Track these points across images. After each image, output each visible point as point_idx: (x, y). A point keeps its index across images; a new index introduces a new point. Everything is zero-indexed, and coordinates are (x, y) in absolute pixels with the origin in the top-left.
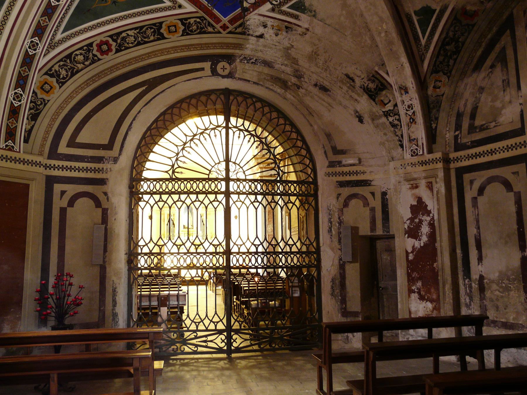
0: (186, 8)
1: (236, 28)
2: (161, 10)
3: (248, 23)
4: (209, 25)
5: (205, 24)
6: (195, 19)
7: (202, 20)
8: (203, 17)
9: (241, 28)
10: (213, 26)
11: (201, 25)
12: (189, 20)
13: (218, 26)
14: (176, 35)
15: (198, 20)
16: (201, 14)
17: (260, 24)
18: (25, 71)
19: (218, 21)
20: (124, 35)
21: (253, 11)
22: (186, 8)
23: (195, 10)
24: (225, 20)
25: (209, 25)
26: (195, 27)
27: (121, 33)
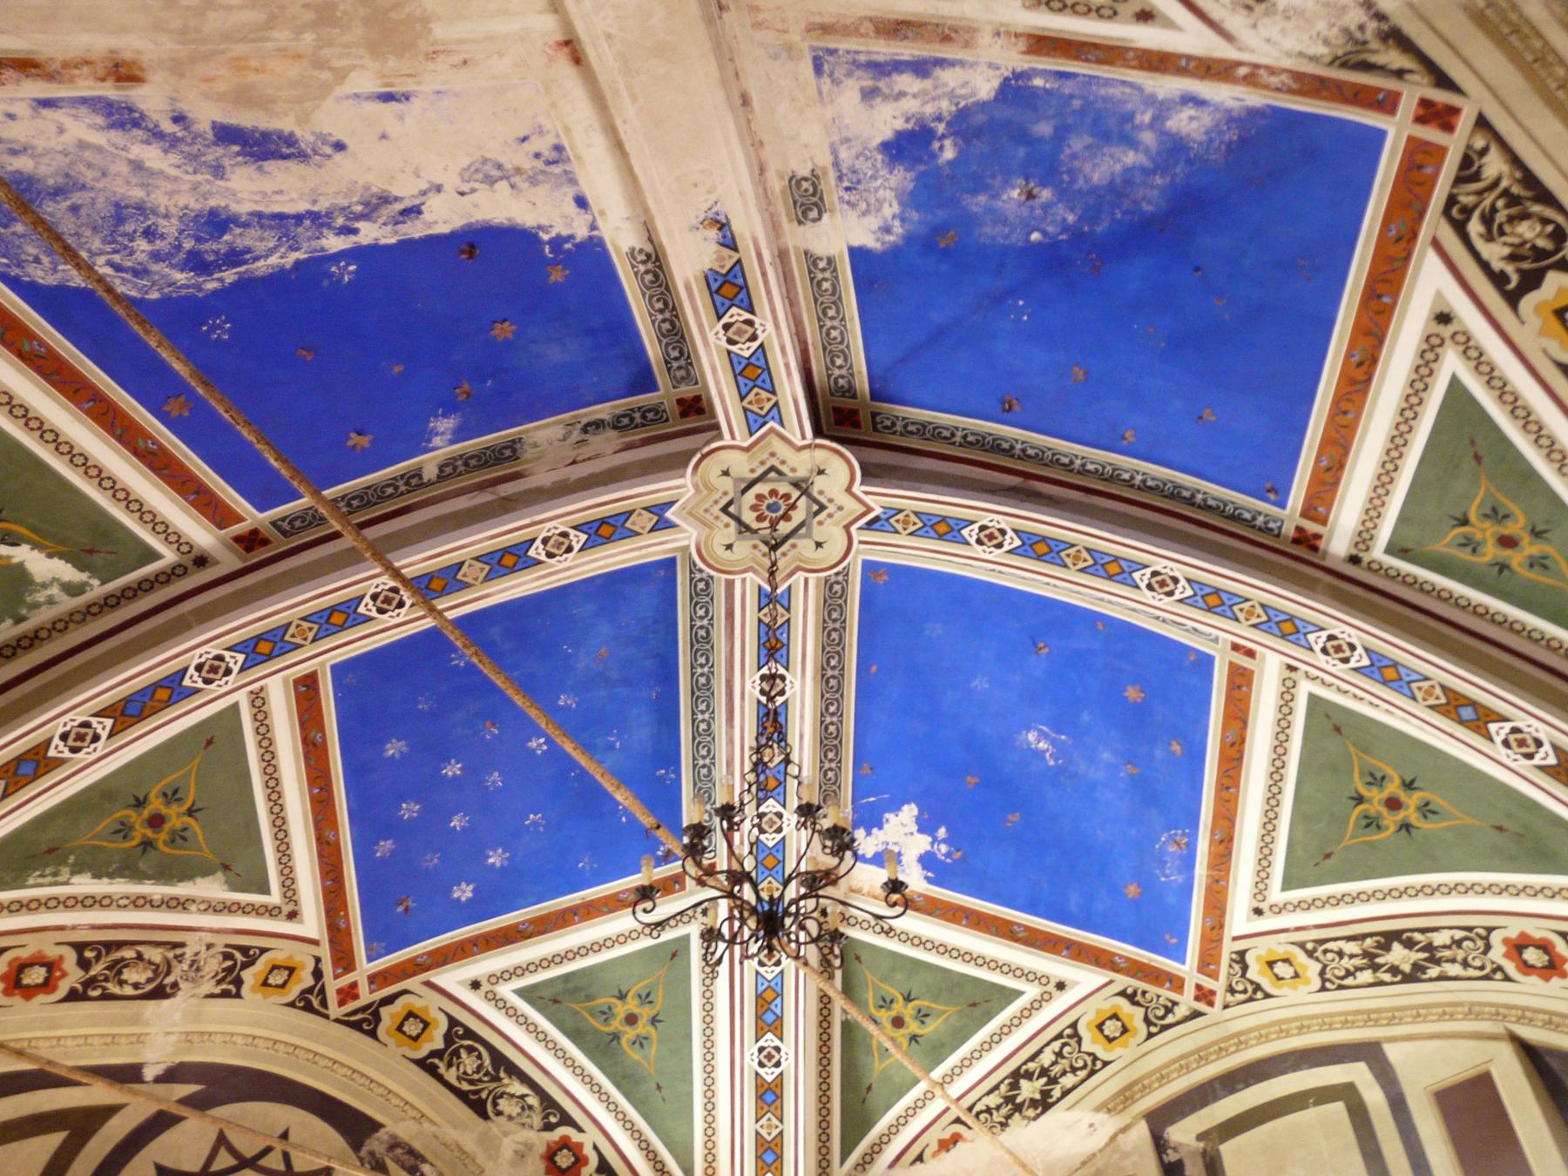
0: (1076, 983)
1: (1400, 74)
2: (824, 1112)
3: (1321, 50)
4: (1476, 177)
5: (1480, 193)
6: (1480, 244)
7: (1467, 211)
8: (1446, 212)
9: (1379, 59)
10: (1466, 161)
11: (1494, 210)
12: (1497, 265)
13: (1455, 144)
14: (575, 1136)
15: (1475, 227)
16: (1433, 223)
17: (1267, 13)
18: (906, 523)
19: (1419, 159)
20: (129, 953)
21: (1239, 64)
22: (1076, 983)
23: (1105, 980)
24: (1188, 969)
25: (1476, 177)
26: (1527, 231)
27: (120, 945)
